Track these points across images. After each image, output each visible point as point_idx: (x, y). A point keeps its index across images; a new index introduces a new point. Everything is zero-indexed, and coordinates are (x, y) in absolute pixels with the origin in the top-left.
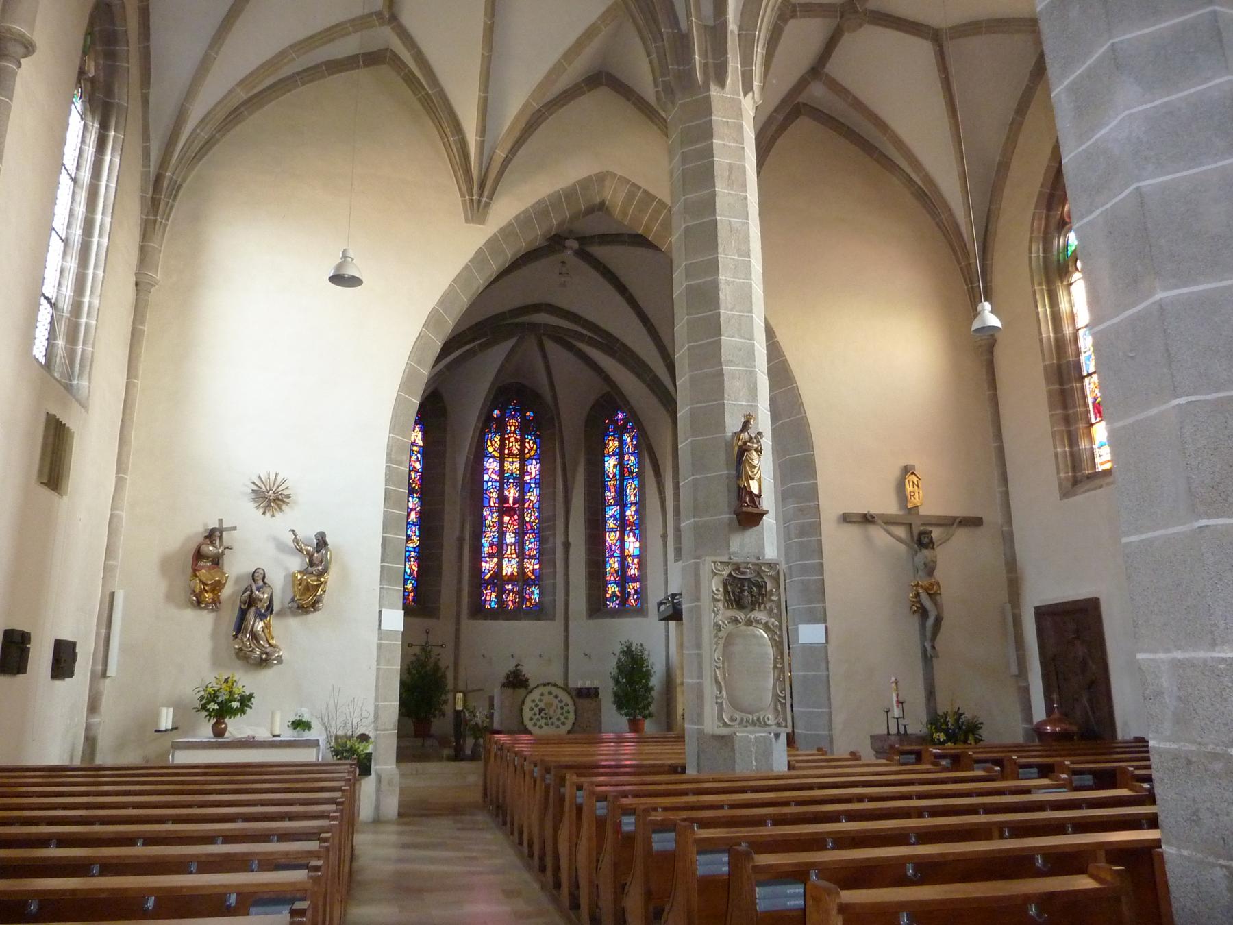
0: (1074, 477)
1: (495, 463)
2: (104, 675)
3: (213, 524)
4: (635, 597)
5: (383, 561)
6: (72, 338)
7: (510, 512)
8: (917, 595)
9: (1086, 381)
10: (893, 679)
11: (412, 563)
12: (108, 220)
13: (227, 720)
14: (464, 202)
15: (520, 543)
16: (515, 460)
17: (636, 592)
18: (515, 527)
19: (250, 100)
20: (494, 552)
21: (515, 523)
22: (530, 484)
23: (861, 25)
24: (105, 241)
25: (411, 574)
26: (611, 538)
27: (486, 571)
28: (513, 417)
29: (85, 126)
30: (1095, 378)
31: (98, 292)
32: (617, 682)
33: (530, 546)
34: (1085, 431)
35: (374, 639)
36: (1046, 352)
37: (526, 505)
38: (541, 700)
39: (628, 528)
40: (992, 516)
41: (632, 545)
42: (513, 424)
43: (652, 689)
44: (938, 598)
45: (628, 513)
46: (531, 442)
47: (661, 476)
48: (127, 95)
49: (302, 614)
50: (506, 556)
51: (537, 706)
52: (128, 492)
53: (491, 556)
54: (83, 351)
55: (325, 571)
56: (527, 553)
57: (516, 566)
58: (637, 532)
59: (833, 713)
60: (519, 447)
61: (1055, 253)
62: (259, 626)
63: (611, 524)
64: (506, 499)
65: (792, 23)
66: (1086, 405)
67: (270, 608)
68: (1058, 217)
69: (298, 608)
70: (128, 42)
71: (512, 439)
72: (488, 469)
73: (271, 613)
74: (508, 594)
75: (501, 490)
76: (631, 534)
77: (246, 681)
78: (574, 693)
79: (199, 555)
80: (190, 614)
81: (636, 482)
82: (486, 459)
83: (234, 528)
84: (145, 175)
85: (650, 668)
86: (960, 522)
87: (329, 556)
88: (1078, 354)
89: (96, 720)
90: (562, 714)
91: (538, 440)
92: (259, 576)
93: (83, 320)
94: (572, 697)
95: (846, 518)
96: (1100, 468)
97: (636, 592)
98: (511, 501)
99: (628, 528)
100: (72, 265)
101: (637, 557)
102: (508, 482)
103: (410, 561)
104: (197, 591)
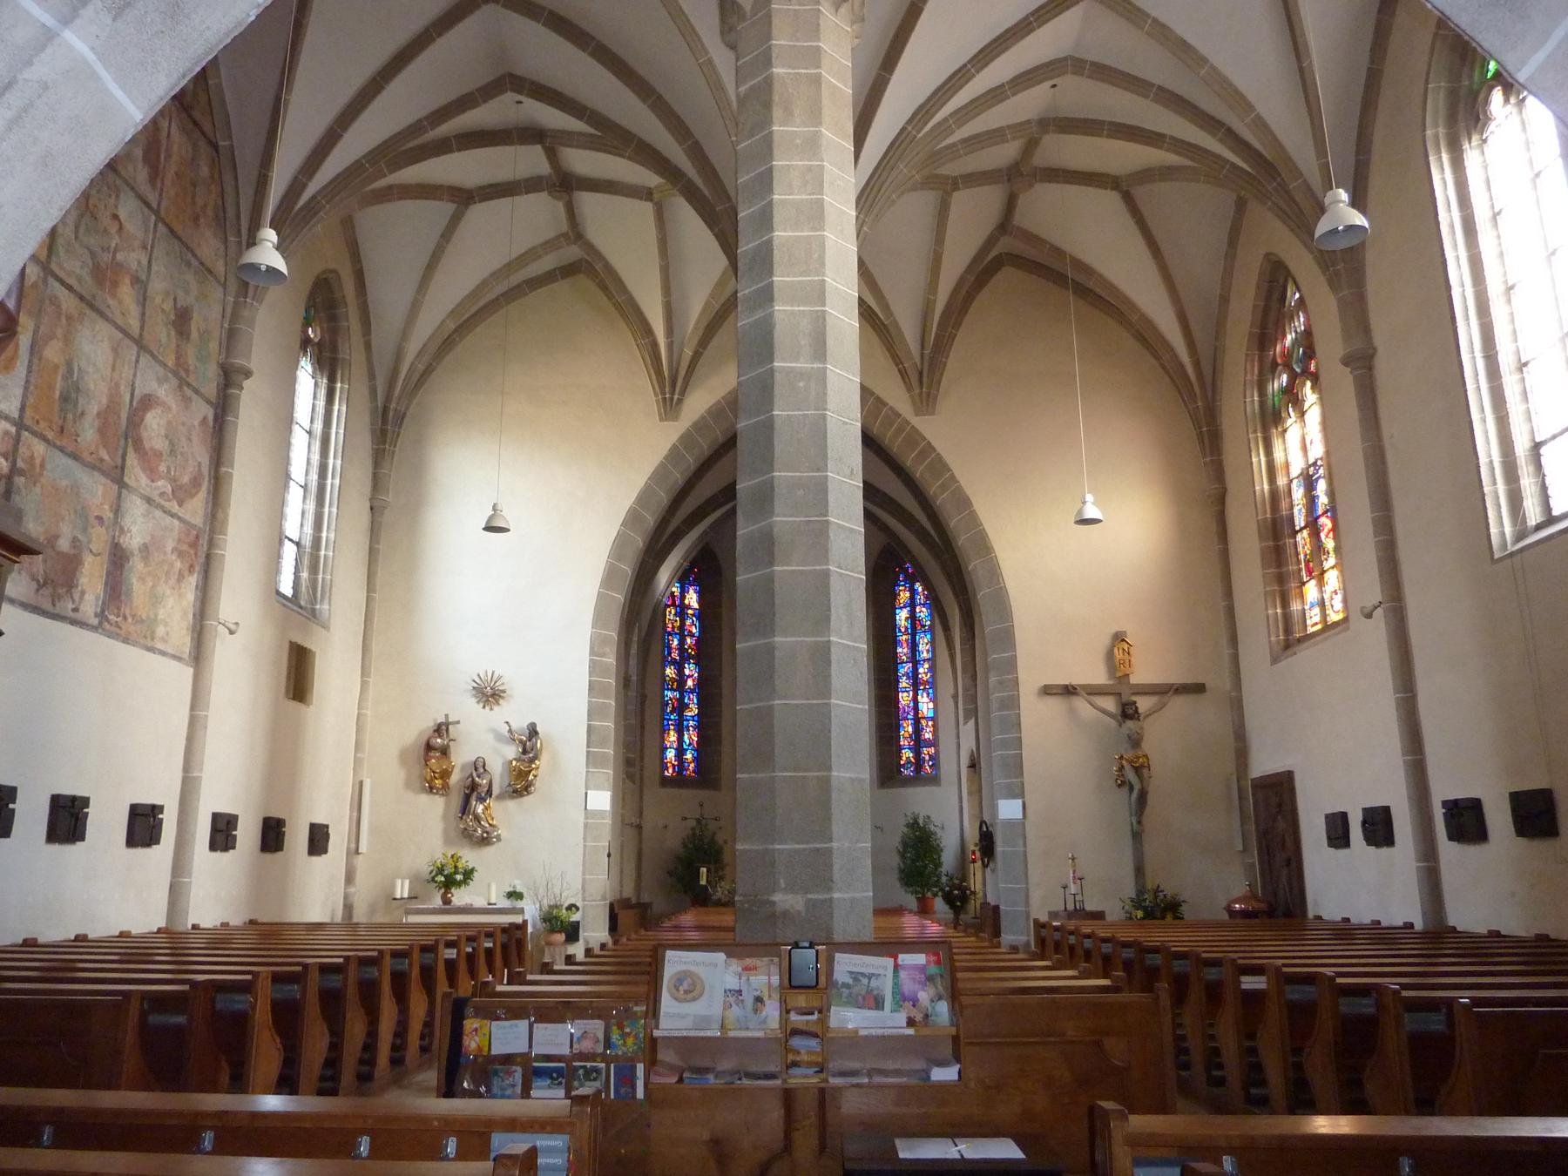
0: (1287, 640)
2: (357, 852)
3: (441, 719)
5: (588, 746)
6: (314, 569)
8: (1121, 768)
9: (1299, 537)
10: (1070, 855)
12: (339, 462)
13: (453, 890)
14: (657, 401)
19: (461, 326)
23: (1031, 186)
24: (337, 481)
25: (690, 744)
26: (905, 699)
29: (316, 384)
30: (1305, 533)
31: (333, 526)
34: (1298, 590)
35: (582, 819)
36: (1259, 506)
40: (1219, 681)
44: (1145, 771)
45: (921, 670)
48: (352, 350)
49: (517, 797)
52: (371, 693)
54: (323, 579)
55: (536, 758)
59: (1031, 889)
61: (1270, 397)
62: (480, 808)
65: (956, 195)
66: (1299, 562)
67: (489, 793)
68: (1271, 357)
69: (514, 792)
70: (346, 304)
73: (491, 796)
76: (925, 695)
77: (469, 857)
79: (429, 747)
80: (425, 798)
81: (929, 636)
83: (458, 722)
84: (374, 411)
86: (1177, 690)
87: (539, 745)
88: (1292, 507)
89: (352, 890)
92: (480, 764)
93: (322, 553)
95: (1047, 691)
96: (1310, 630)
100: (311, 506)
101: (932, 719)
103: (688, 730)
104: (428, 778)
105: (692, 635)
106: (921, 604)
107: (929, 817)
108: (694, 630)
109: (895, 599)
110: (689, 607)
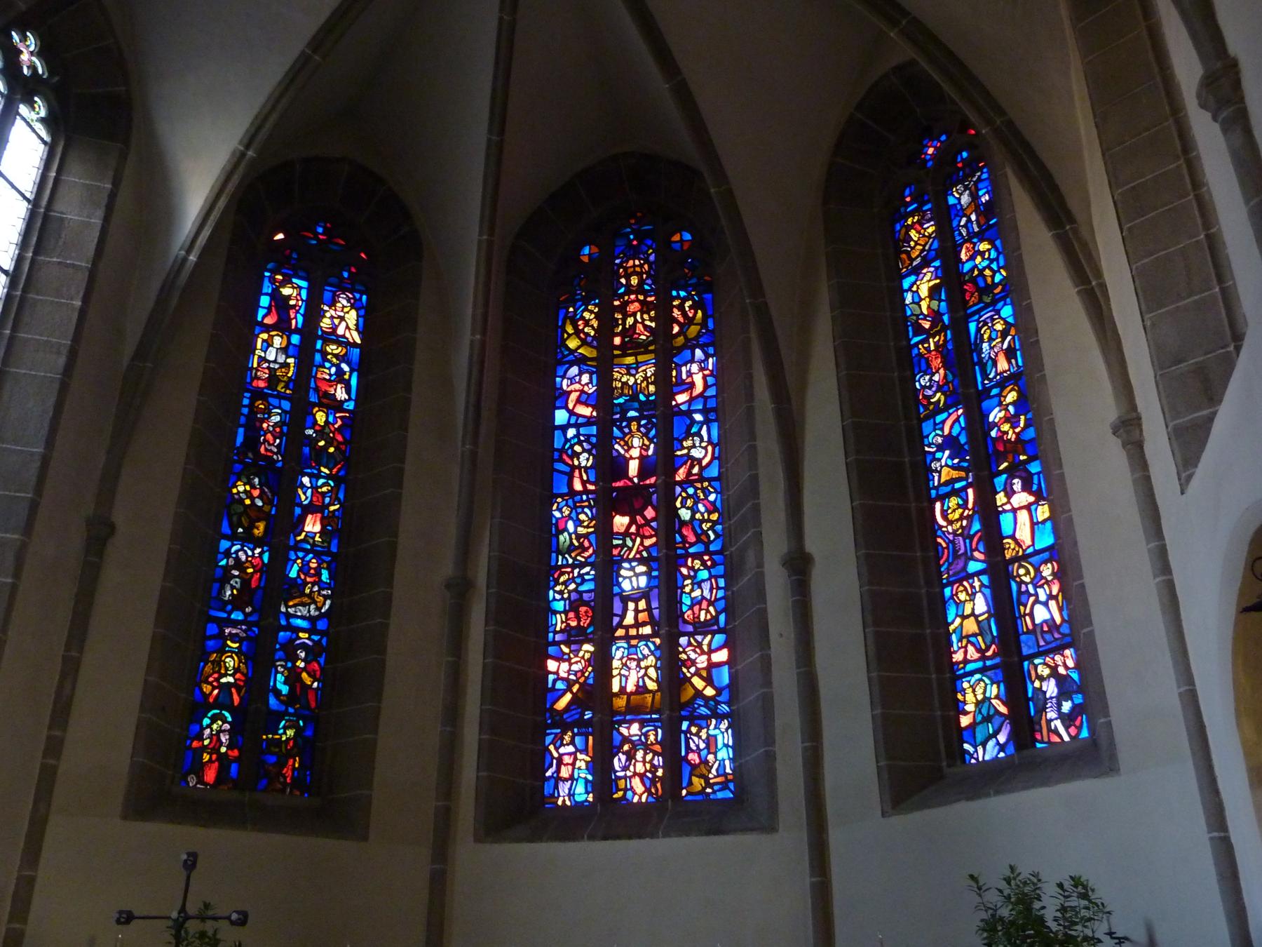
4: (1067, 706)
7: (630, 501)
16: (640, 358)
20: (583, 623)
21: (648, 532)
25: (292, 698)
33: (697, 593)
37: (681, 475)
41: (1023, 516)
45: (995, 415)
47: (1072, 220)
50: (620, 632)
53: (574, 637)
56: (688, 615)
57: (651, 660)
58: (1035, 468)
63: (944, 468)
74: (630, 756)
76: (1017, 484)
91: (708, 296)
98: (633, 467)
101: (1052, 553)
102: (624, 417)
105: (333, 405)
106: (971, 235)
107: (1081, 887)
108: (341, 394)
109: (898, 252)
110: (331, 337)
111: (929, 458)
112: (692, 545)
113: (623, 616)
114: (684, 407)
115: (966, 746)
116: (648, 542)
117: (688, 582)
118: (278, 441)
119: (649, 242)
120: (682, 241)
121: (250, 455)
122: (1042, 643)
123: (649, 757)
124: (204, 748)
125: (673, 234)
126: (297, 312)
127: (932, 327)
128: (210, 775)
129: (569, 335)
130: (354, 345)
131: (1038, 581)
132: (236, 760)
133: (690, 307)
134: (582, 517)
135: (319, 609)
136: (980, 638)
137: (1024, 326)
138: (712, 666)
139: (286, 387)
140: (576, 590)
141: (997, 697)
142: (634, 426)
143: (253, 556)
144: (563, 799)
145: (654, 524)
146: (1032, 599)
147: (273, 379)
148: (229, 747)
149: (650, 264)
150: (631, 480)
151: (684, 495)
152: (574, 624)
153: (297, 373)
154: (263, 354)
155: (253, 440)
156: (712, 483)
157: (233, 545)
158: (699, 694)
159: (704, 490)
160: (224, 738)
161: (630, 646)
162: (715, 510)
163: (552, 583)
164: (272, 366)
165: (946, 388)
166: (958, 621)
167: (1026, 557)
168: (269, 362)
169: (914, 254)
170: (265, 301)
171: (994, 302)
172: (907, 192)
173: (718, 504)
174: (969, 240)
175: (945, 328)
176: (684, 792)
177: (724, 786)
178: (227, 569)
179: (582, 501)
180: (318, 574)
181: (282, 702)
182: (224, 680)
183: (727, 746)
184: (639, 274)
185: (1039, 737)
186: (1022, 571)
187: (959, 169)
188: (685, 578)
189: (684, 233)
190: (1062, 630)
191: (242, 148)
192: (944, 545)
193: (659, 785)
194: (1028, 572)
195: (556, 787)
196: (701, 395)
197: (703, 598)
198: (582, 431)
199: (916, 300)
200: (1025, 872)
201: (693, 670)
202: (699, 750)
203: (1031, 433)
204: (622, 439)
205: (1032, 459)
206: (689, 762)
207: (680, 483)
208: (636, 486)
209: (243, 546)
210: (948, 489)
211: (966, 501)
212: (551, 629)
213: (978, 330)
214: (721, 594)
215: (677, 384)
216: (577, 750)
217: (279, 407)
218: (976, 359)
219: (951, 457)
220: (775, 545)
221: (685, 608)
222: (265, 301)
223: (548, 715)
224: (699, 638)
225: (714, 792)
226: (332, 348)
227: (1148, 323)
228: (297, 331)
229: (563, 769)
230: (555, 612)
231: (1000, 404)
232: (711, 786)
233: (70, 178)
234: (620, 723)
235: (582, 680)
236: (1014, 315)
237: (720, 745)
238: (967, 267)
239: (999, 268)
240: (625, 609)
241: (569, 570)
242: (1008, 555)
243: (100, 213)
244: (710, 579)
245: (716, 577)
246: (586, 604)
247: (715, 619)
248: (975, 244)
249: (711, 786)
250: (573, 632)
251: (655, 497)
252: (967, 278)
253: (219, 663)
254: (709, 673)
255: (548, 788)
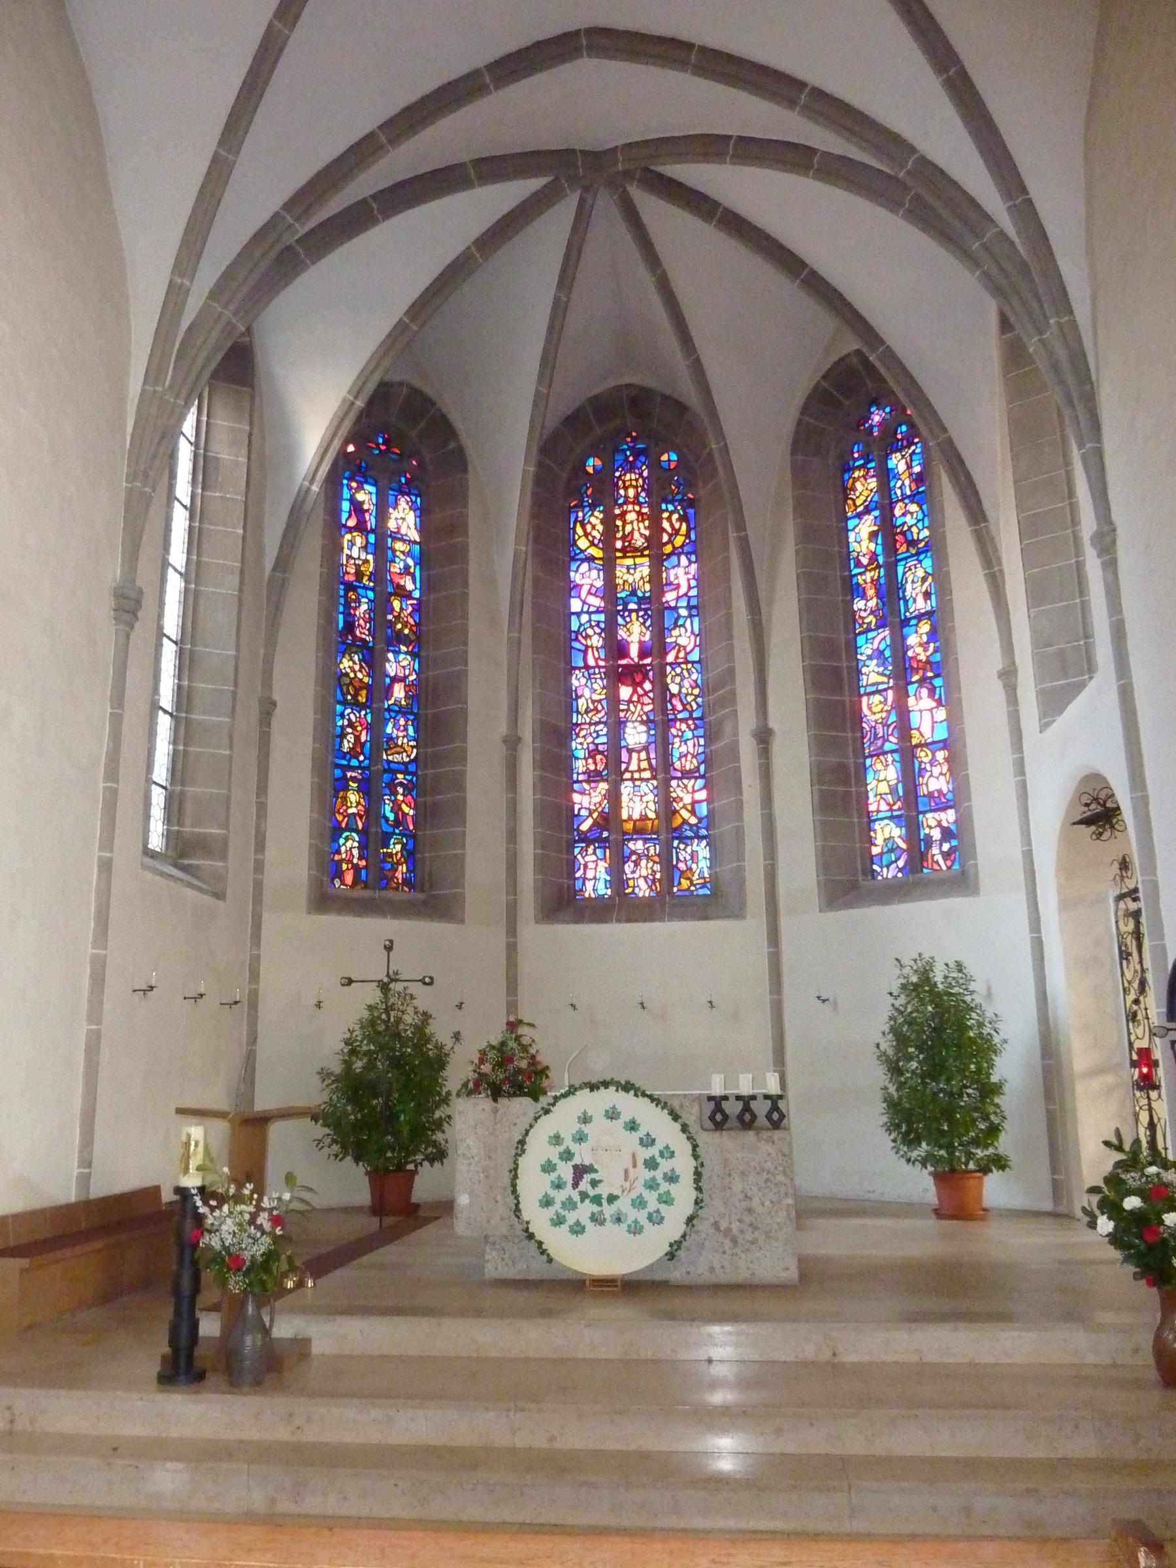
1: (594, 573)
4: (946, 847)
7: (633, 675)
11: (400, 798)
15: (662, 743)
16: (638, 561)
17: (947, 834)
18: (647, 708)
20: (600, 767)
21: (646, 700)
22: (676, 608)
25: (397, 823)
26: (874, 709)
27: (584, 813)
28: (632, 467)
32: (895, 1070)
33: (684, 749)
37: (670, 658)
38: (580, 1138)
39: (916, 678)
42: (631, 483)
43: (997, 1089)
45: (912, 640)
46: (675, 517)
47: (985, 519)
50: (627, 775)
51: (567, 1155)
53: (593, 777)
56: (677, 765)
57: (651, 797)
60: (647, 533)
63: (872, 673)
64: (621, 649)
71: (631, 516)
72: (579, 587)
74: (637, 864)
75: (610, 629)
76: (924, 692)
78: (691, 1116)
82: (574, 566)
85: (987, 1030)
90: (652, 1185)
91: (691, 511)
94: (685, 1128)
97: (947, 834)
98: (634, 651)
99: (916, 678)
101: (945, 744)
102: (625, 609)
103: (395, 793)
108: (409, 586)
109: (846, 498)
110: (397, 536)
111: (861, 664)
112: (680, 712)
113: (629, 764)
114: (673, 604)
115: (875, 867)
116: (647, 708)
117: (677, 740)
118: (368, 625)
119: (643, 459)
120: (669, 460)
121: (350, 637)
122: (933, 804)
123: (650, 864)
124: (342, 860)
125: (662, 454)
126: (371, 514)
127: (869, 565)
128: (349, 878)
129: (580, 537)
130: (415, 542)
131: (932, 762)
132: (366, 867)
133: (677, 520)
134: (595, 686)
135: (408, 756)
136: (889, 796)
137: (940, 581)
138: (694, 802)
139: (370, 580)
140: (593, 743)
141: (900, 837)
142: (634, 615)
143: (360, 717)
144: (589, 891)
145: (651, 695)
146: (928, 774)
147: (359, 574)
148: (360, 859)
149: (644, 479)
150: (632, 659)
151: (673, 673)
152: (592, 767)
153: (375, 567)
154: (349, 553)
155: (350, 626)
156: (695, 665)
157: (345, 709)
158: (685, 822)
159: (688, 670)
160: (355, 852)
161: (635, 786)
162: (697, 686)
163: (574, 737)
164: (357, 562)
165: (877, 613)
166: (875, 782)
167: (927, 745)
168: (355, 559)
169: (858, 502)
170: (346, 506)
171: (918, 554)
172: (856, 449)
173: (699, 682)
174: (902, 500)
175: (879, 567)
176: (675, 889)
177: (703, 886)
178: (343, 727)
179: (594, 674)
180: (406, 729)
181: (391, 826)
182: (350, 811)
183: (705, 858)
184: (636, 487)
185: (925, 865)
186: (923, 754)
187: (898, 440)
188: (674, 737)
189: (671, 453)
190: (947, 797)
191: (351, 398)
192: (868, 729)
193: (658, 884)
194: (927, 755)
195: (584, 884)
196: (686, 595)
197: (688, 752)
198: (594, 617)
199: (858, 540)
200: (926, 956)
201: (681, 804)
202: (686, 861)
203: (937, 657)
204: (624, 626)
205: (937, 676)
206: (679, 869)
207: (670, 664)
208: (637, 665)
209: (352, 709)
210: (874, 689)
211: (886, 700)
212: (575, 771)
213: (904, 573)
214: (701, 750)
215: (667, 584)
216: (598, 859)
217: (367, 597)
218: (901, 595)
219: (878, 665)
220: (747, 721)
221: (675, 760)
222: (346, 506)
223: (575, 833)
224: (686, 781)
225: (697, 889)
226: (399, 546)
227: (1032, 615)
228: (372, 531)
229: (588, 871)
230: (577, 758)
231: (916, 632)
232: (695, 885)
233: (219, 422)
234: (629, 840)
235: (600, 810)
236: (933, 566)
237: (700, 857)
238: (899, 522)
239: (924, 528)
240: (630, 758)
241: (587, 726)
242: (914, 742)
243: (244, 452)
244: (693, 738)
245: (698, 737)
246: (601, 753)
247: (698, 768)
248: (906, 505)
249: (695, 885)
250: (592, 774)
251: (651, 673)
252: (898, 530)
253: (345, 798)
254: (693, 808)
255: (578, 885)
